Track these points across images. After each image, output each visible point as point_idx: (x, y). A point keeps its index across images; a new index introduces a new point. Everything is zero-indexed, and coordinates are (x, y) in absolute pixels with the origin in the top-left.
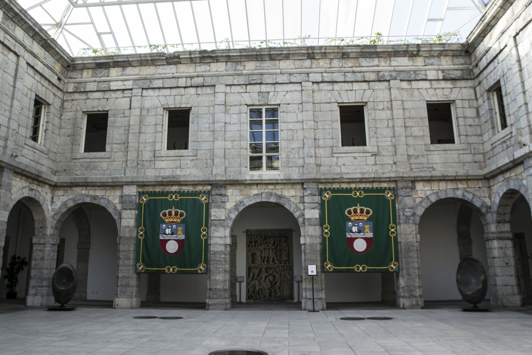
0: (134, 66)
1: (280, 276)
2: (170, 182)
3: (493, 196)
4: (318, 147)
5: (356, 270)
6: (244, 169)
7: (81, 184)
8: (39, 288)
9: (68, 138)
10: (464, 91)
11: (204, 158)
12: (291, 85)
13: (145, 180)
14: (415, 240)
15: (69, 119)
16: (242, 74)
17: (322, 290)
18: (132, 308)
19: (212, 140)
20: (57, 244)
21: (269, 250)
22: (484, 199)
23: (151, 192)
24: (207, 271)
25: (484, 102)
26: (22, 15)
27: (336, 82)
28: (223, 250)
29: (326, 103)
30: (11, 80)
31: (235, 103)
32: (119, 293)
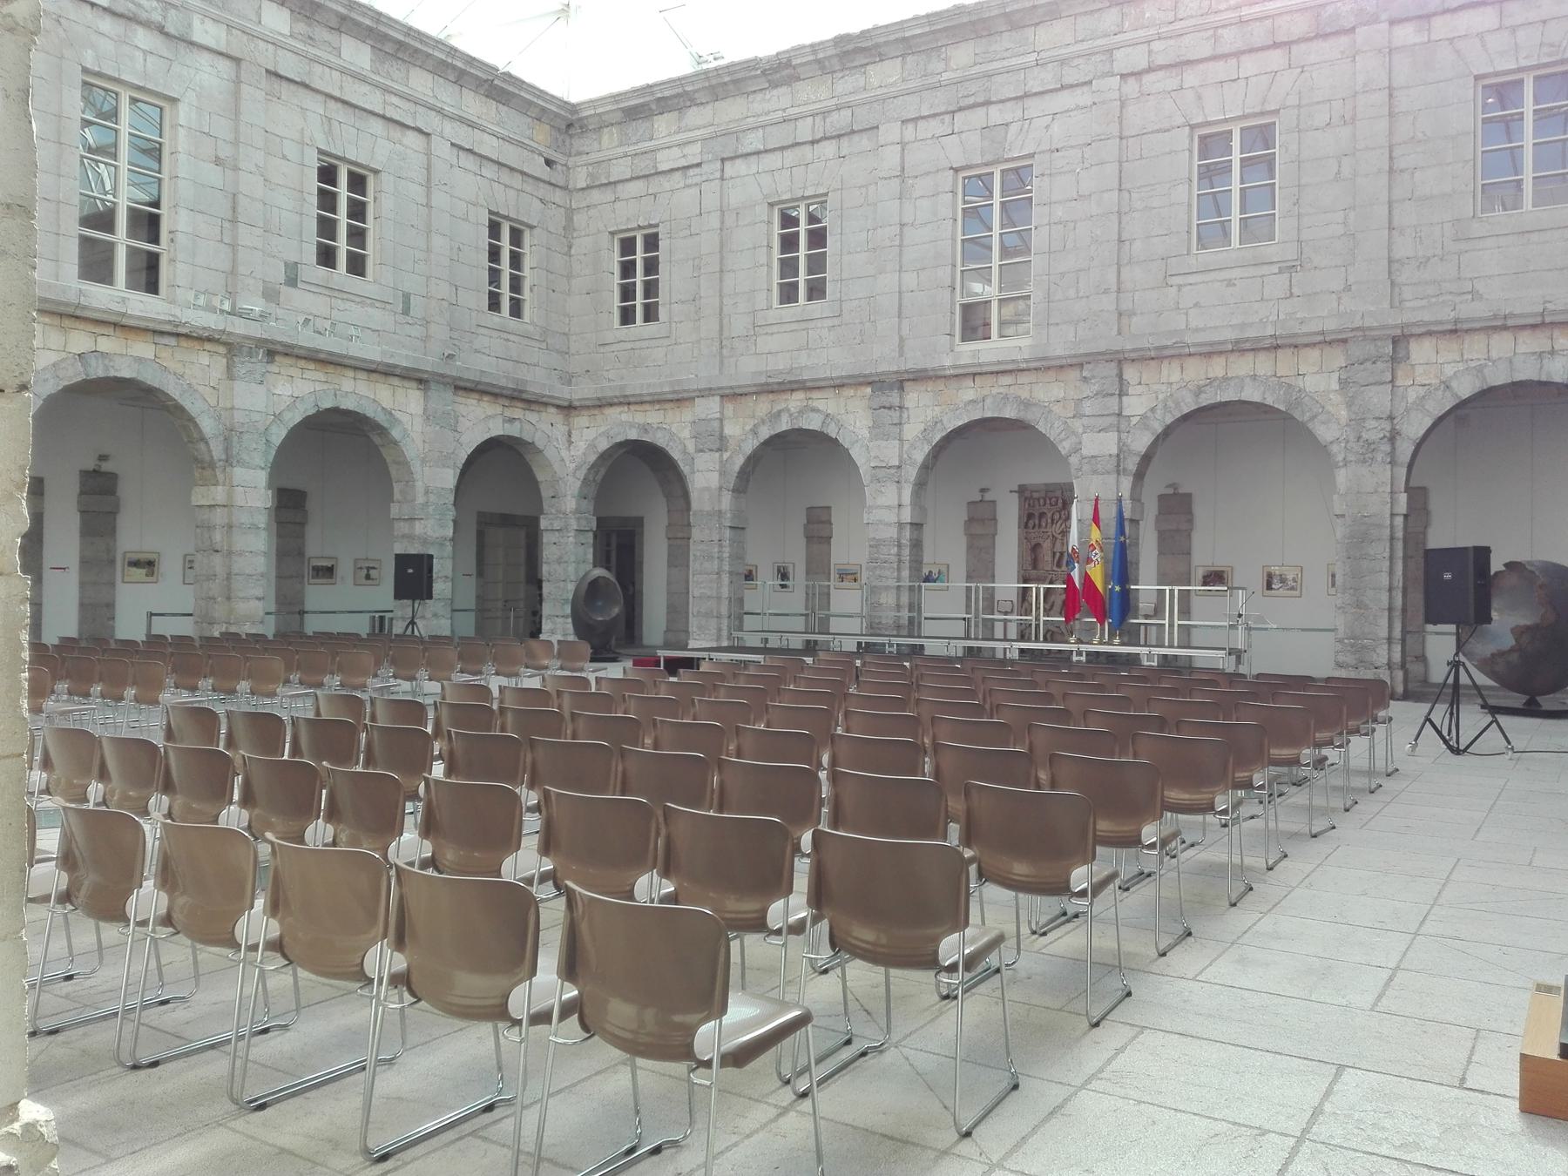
0: (702, 104)
11: (857, 321)
12: (1065, 94)
20: (591, 530)
26: (412, 43)
29: (1158, 131)
30: (417, 192)
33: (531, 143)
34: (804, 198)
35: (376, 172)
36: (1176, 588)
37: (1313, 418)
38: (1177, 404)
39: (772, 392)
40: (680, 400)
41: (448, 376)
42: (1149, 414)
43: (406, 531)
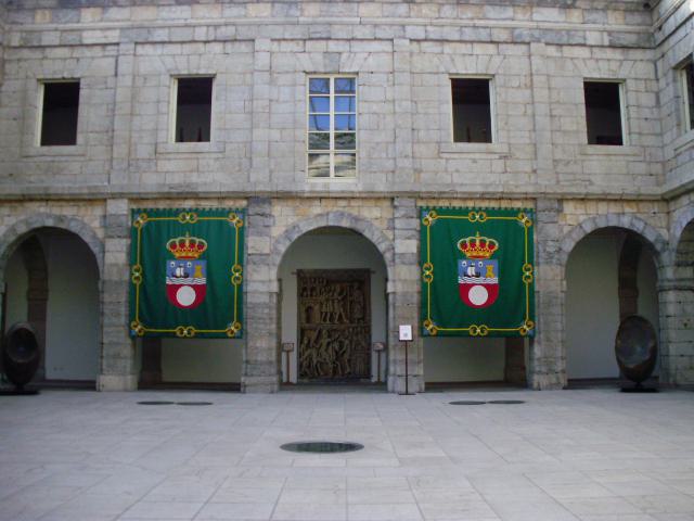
1: (351, 342)
2: (181, 193)
3: (672, 226)
4: (418, 142)
5: (471, 333)
6: (299, 174)
9: (14, 123)
10: (640, 65)
13: (142, 191)
14: (559, 289)
16: (298, 23)
17: (419, 363)
18: (126, 390)
19: (249, 126)
23: (152, 209)
24: (242, 333)
25: (668, 85)
27: (447, 41)
28: (267, 301)
29: (430, 73)
31: (286, 69)
32: (104, 367)
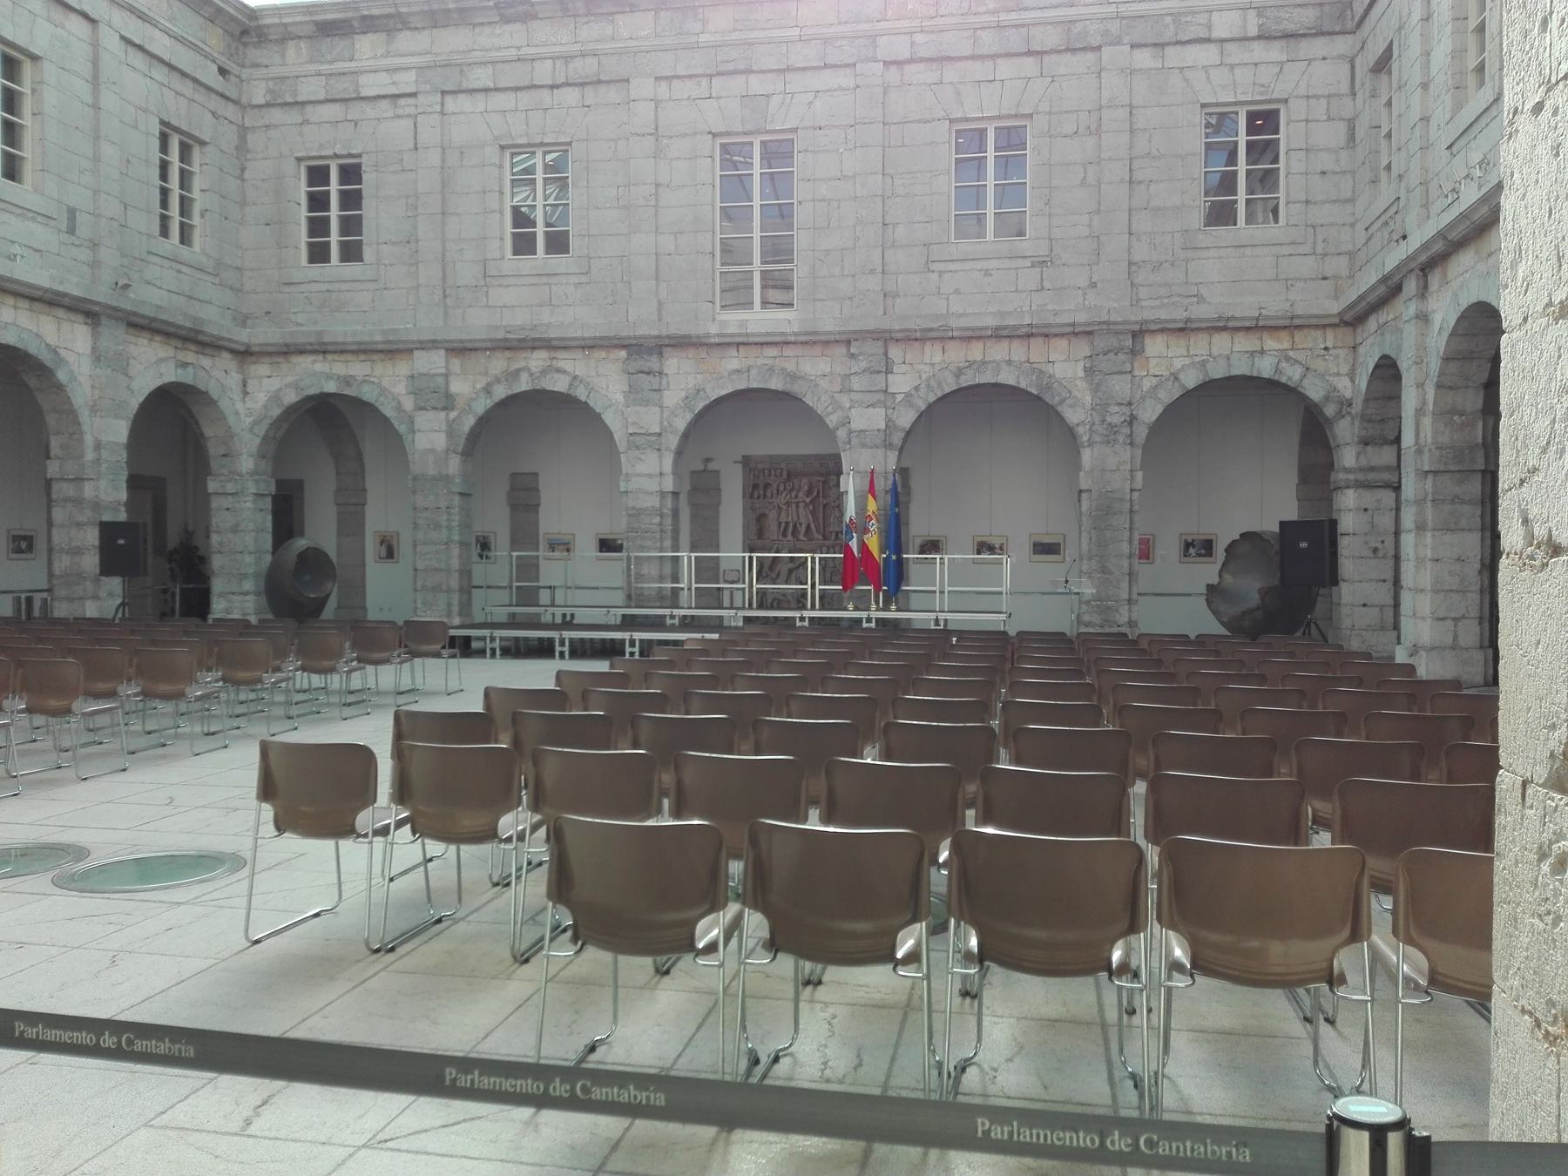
0: (417, 29)
2: (524, 340)
7: (309, 348)
8: (235, 598)
13: (464, 336)
15: (263, 180)
21: (797, 507)
22: (1335, 381)
27: (950, 59)
29: (919, 121)
30: (82, 88)
33: (204, 46)
34: (542, 144)
35: (34, 58)
36: (817, 556)
37: (1062, 402)
38: (939, 384)
39: (508, 349)
40: (392, 351)
41: (121, 310)
42: (913, 392)
43: (71, 493)
